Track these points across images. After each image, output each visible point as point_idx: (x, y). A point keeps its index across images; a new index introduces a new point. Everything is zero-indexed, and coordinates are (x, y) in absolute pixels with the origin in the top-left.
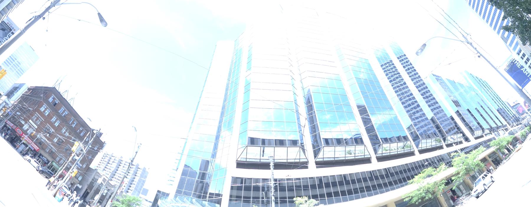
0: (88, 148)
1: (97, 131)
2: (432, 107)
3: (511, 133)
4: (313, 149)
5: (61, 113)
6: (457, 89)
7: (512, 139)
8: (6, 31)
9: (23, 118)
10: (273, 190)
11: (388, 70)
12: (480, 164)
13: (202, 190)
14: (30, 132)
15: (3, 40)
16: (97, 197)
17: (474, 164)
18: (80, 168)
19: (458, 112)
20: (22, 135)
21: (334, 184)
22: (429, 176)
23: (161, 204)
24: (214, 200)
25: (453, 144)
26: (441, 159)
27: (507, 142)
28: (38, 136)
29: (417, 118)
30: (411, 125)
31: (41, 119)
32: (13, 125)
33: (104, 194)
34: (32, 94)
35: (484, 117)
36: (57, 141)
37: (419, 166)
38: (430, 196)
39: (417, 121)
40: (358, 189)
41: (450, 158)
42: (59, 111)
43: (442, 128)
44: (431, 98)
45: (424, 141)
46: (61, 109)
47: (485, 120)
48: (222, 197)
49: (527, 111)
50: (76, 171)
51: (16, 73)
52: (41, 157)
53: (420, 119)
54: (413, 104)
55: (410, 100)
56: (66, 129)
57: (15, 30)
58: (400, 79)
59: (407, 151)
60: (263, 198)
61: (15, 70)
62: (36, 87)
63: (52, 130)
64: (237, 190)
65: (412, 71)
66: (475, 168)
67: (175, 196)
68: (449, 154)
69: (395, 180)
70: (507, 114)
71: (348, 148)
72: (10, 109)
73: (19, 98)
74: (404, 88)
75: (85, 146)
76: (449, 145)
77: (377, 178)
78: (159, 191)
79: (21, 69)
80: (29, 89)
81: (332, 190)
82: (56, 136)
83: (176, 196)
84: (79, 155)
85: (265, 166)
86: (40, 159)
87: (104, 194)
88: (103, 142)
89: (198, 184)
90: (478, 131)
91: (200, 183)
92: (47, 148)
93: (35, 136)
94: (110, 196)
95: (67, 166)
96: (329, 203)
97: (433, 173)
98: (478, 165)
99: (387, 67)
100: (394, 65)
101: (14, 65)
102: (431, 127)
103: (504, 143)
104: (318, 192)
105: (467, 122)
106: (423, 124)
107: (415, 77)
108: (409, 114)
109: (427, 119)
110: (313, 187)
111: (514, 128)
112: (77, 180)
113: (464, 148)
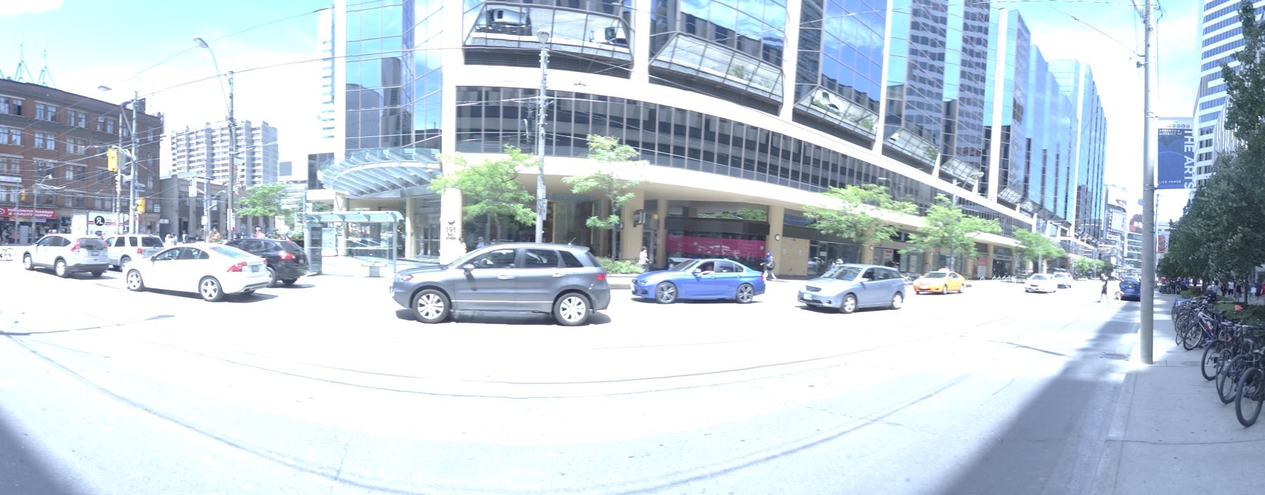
2: (967, 82)
3: (1065, 245)
4: (652, 32)
6: (1040, 87)
7: (1059, 255)
12: (970, 248)
14: (16, 197)
16: (205, 220)
19: (1007, 129)
20: (7, 213)
23: (324, 177)
25: (955, 181)
27: (1044, 253)
28: (35, 192)
29: (922, 80)
30: (901, 86)
33: (215, 209)
38: (853, 235)
39: (918, 85)
41: (931, 201)
42: (37, 117)
45: (906, 136)
46: (38, 110)
47: (1043, 184)
50: (140, 201)
53: (927, 87)
59: (859, 132)
66: (956, 247)
67: (346, 155)
68: (934, 191)
69: (806, 172)
70: (1088, 208)
71: (739, 61)
76: (944, 176)
77: (775, 152)
78: (311, 157)
81: (672, 140)
82: (65, 168)
83: (348, 155)
84: (128, 172)
88: (156, 115)
90: (1012, 193)
91: (391, 115)
93: (30, 197)
95: (121, 205)
96: (660, 163)
98: (965, 246)
102: (935, 118)
103: (1040, 251)
109: (940, 96)
111: (1079, 241)
113: (967, 201)
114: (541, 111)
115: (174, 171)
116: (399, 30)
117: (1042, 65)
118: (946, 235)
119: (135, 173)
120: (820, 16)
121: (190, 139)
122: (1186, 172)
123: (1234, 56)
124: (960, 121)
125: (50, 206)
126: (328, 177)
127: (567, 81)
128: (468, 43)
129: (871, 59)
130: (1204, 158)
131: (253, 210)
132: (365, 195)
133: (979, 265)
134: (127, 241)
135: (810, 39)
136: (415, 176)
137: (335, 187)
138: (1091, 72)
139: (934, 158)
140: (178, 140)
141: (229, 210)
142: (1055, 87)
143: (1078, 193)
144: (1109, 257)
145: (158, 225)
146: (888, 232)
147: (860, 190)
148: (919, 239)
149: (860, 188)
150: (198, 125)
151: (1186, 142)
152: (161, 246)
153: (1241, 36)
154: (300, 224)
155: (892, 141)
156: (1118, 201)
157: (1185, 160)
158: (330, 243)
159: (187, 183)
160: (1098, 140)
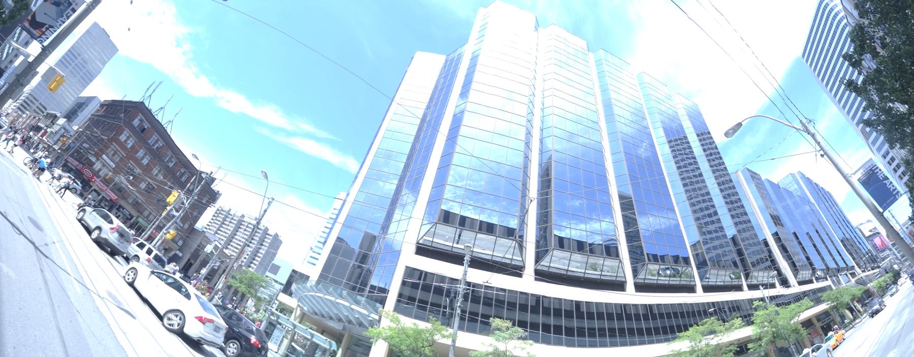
0: (193, 201)
1: (207, 174)
2: (737, 220)
5: (151, 144)
6: (781, 198)
7: (861, 292)
8: (62, 7)
9: (93, 153)
10: (460, 299)
11: (678, 150)
13: (359, 278)
15: (58, 24)
16: (204, 271)
17: (789, 328)
18: (180, 228)
19: (776, 235)
20: (92, 178)
21: (558, 313)
22: (712, 332)
24: (375, 297)
25: (761, 287)
26: (735, 307)
27: (851, 297)
29: (710, 232)
31: (121, 153)
32: (78, 163)
33: (216, 268)
34: (107, 113)
35: (819, 249)
36: (146, 187)
37: (699, 312)
39: (708, 236)
40: (597, 330)
43: (746, 256)
44: (739, 204)
45: (714, 272)
47: (819, 254)
48: (388, 294)
49: (891, 247)
51: (81, 79)
52: (121, 209)
53: (714, 235)
54: (707, 209)
55: (704, 201)
56: (159, 169)
57: (77, 4)
58: (695, 166)
59: (684, 283)
60: (445, 307)
61: (79, 74)
62: (114, 101)
63: (138, 171)
64: (412, 287)
65: (717, 158)
68: (751, 301)
70: (856, 248)
71: (592, 260)
72: (73, 138)
73: (86, 120)
74: (697, 182)
75: (187, 197)
76: (752, 287)
77: (629, 317)
78: (294, 271)
79: (88, 72)
80: (102, 105)
82: (143, 180)
83: (318, 282)
85: (455, 258)
86: (119, 213)
87: (216, 268)
88: (216, 192)
89: (355, 269)
90: (804, 272)
92: (131, 197)
93: (111, 180)
94: (224, 271)
97: (718, 328)
98: (796, 331)
99: (678, 145)
100: (689, 143)
101: (76, 64)
103: (846, 299)
104: (529, 317)
105: (790, 253)
106: (717, 243)
107: (719, 168)
108: (704, 239)
109: (725, 236)
110: (523, 308)
111: (867, 273)
112: (175, 245)
113: (776, 296)
114: (460, 295)
115: (206, 228)
116: (381, 221)
117: (775, 187)
118: (774, 329)
119: (181, 214)
120: (635, 220)
121: (227, 217)
122: (891, 190)
123: (864, 111)
124: (744, 245)
125: (118, 193)
126: (298, 291)
127: (478, 276)
128: (420, 242)
129: (674, 233)
130: (897, 169)
131: (239, 285)
132: (318, 317)
133: (813, 339)
134: (146, 249)
135: (633, 237)
136: (358, 318)
137: (299, 300)
138: (802, 174)
139: (739, 278)
140: (220, 213)
141: (223, 276)
142: (790, 194)
143: (843, 245)
144: (892, 267)
145: (173, 253)
146: (731, 351)
147: (698, 327)
148: (756, 345)
149: (698, 326)
150: (237, 211)
151: (878, 174)
152: (163, 266)
153: (859, 99)
154: (264, 312)
155: (707, 280)
156: (870, 231)
157: (886, 184)
158: (277, 340)
159: (209, 242)
160: (832, 206)
